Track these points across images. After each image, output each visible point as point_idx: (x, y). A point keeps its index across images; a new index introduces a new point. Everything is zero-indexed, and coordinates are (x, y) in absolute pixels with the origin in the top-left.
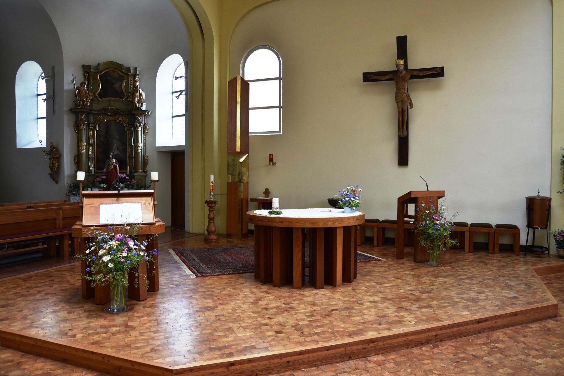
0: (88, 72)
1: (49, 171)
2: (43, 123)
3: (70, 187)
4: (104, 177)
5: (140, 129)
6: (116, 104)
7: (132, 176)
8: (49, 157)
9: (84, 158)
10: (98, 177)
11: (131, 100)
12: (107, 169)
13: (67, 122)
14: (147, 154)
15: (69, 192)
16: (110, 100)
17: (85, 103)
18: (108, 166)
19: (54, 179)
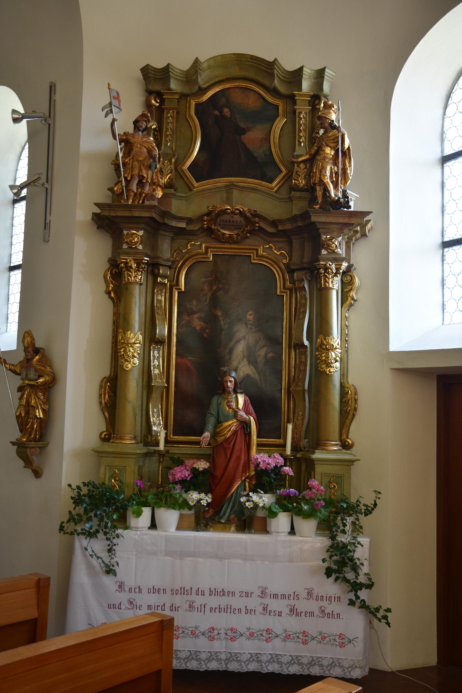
0: (159, 95)
1: (16, 434)
2: (17, 276)
3: (77, 501)
4: (202, 465)
5: (335, 284)
6: (257, 198)
7: (303, 464)
8: (18, 381)
9: (133, 389)
10: (179, 462)
11: (302, 182)
12: (214, 435)
13: (85, 256)
14: (351, 380)
15: (72, 519)
16: (229, 187)
17: (147, 189)
18: (219, 422)
19: (28, 463)
